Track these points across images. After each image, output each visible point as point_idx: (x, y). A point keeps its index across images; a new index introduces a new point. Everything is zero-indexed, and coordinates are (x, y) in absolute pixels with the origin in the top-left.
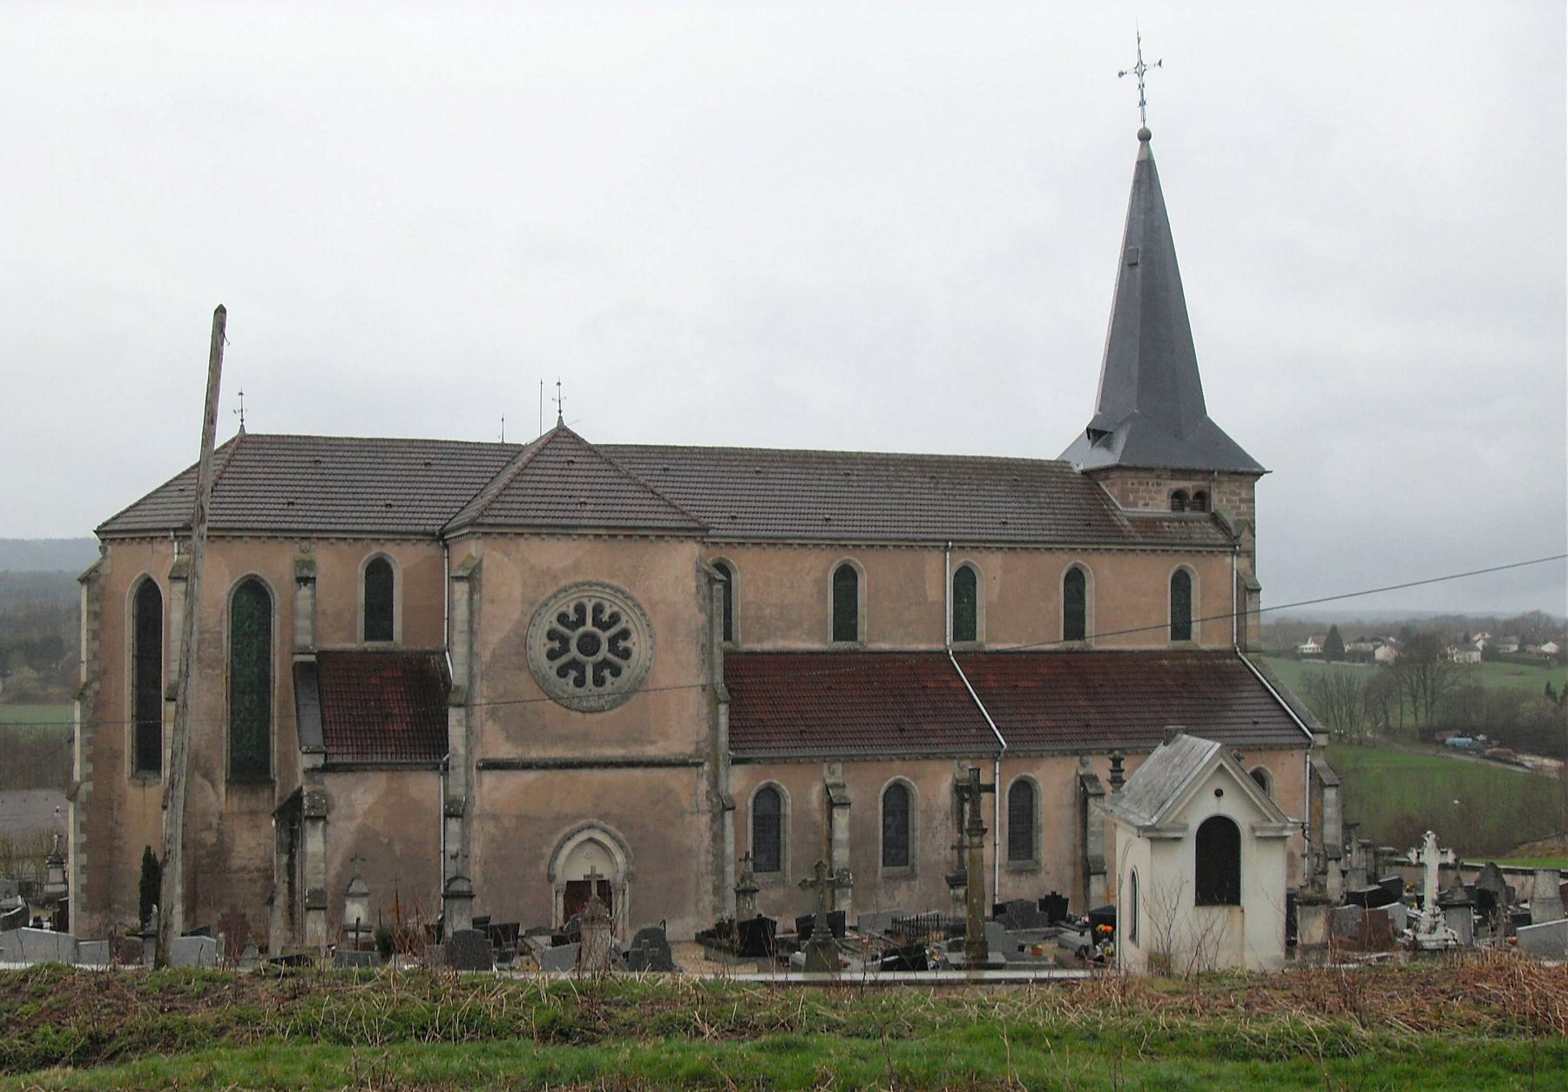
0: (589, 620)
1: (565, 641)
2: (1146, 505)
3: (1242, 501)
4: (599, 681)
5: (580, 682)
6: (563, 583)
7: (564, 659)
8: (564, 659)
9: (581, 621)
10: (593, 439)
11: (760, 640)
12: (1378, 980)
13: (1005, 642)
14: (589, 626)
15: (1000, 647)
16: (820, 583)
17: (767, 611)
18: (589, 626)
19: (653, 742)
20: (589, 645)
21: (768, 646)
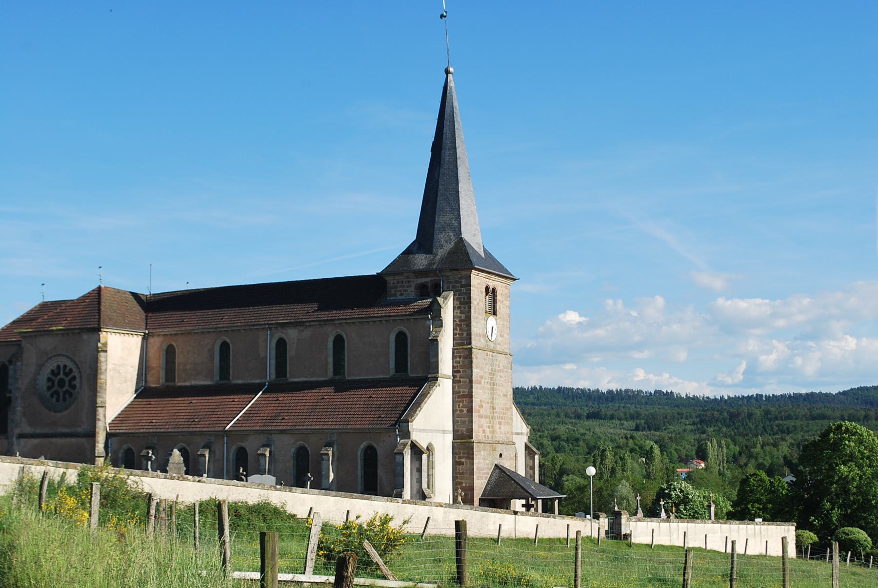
0: (62, 373)
1: (53, 381)
2: (402, 295)
3: (462, 286)
4: (65, 400)
5: (58, 400)
6: (50, 355)
7: (53, 390)
8: (53, 390)
9: (59, 374)
10: (75, 297)
11: (185, 381)
12: (124, 576)
13: (299, 377)
14: (61, 376)
15: (296, 380)
16: (211, 352)
17: (188, 367)
18: (61, 376)
19: (80, 426)
20: (62, 383)
21: (188, 384)
